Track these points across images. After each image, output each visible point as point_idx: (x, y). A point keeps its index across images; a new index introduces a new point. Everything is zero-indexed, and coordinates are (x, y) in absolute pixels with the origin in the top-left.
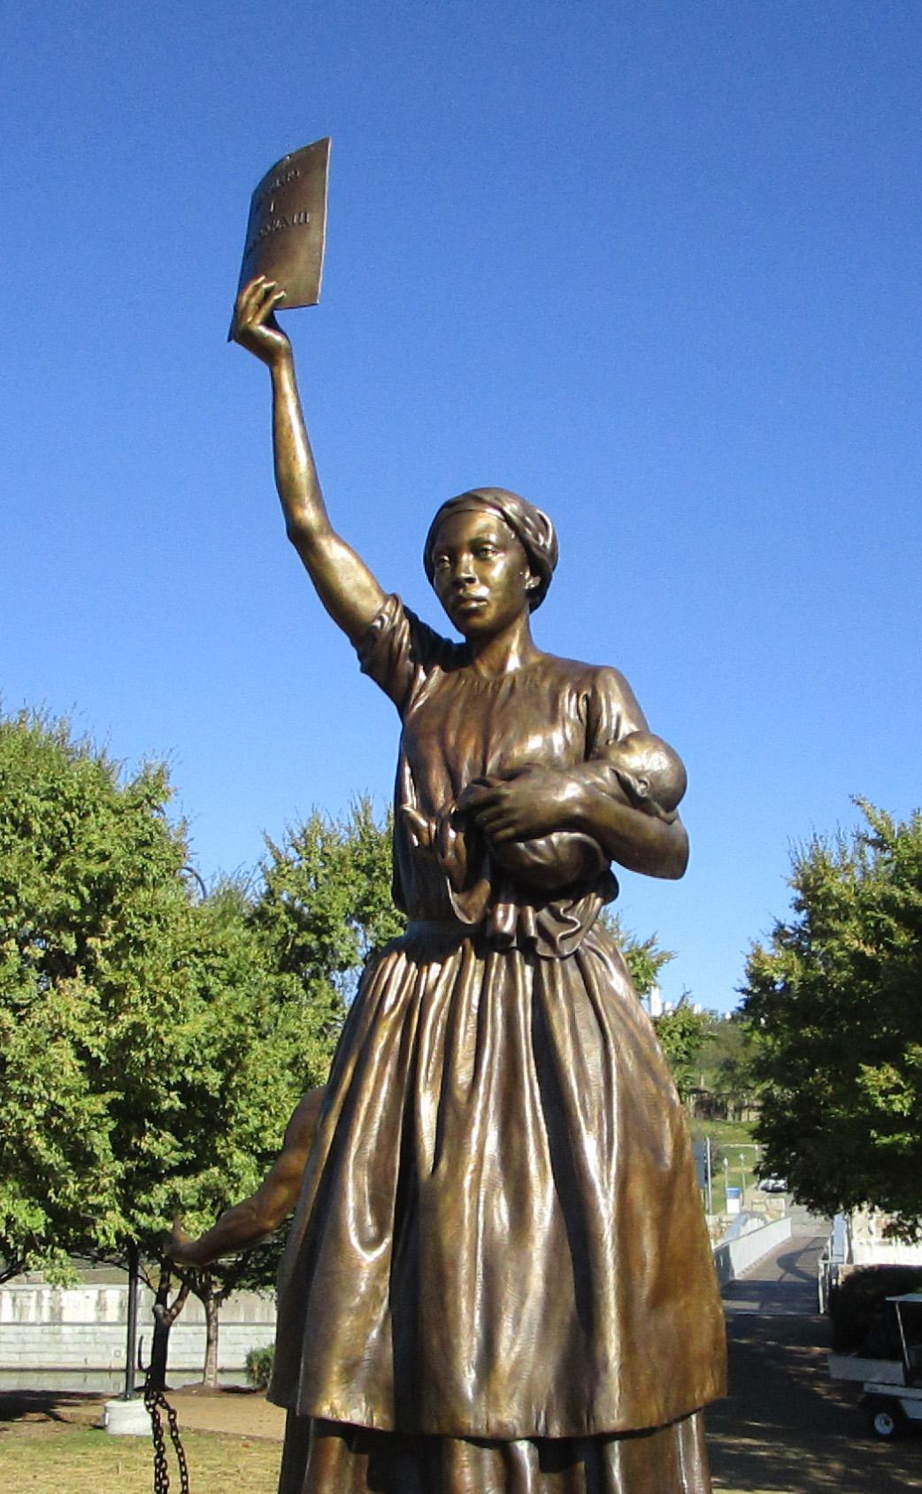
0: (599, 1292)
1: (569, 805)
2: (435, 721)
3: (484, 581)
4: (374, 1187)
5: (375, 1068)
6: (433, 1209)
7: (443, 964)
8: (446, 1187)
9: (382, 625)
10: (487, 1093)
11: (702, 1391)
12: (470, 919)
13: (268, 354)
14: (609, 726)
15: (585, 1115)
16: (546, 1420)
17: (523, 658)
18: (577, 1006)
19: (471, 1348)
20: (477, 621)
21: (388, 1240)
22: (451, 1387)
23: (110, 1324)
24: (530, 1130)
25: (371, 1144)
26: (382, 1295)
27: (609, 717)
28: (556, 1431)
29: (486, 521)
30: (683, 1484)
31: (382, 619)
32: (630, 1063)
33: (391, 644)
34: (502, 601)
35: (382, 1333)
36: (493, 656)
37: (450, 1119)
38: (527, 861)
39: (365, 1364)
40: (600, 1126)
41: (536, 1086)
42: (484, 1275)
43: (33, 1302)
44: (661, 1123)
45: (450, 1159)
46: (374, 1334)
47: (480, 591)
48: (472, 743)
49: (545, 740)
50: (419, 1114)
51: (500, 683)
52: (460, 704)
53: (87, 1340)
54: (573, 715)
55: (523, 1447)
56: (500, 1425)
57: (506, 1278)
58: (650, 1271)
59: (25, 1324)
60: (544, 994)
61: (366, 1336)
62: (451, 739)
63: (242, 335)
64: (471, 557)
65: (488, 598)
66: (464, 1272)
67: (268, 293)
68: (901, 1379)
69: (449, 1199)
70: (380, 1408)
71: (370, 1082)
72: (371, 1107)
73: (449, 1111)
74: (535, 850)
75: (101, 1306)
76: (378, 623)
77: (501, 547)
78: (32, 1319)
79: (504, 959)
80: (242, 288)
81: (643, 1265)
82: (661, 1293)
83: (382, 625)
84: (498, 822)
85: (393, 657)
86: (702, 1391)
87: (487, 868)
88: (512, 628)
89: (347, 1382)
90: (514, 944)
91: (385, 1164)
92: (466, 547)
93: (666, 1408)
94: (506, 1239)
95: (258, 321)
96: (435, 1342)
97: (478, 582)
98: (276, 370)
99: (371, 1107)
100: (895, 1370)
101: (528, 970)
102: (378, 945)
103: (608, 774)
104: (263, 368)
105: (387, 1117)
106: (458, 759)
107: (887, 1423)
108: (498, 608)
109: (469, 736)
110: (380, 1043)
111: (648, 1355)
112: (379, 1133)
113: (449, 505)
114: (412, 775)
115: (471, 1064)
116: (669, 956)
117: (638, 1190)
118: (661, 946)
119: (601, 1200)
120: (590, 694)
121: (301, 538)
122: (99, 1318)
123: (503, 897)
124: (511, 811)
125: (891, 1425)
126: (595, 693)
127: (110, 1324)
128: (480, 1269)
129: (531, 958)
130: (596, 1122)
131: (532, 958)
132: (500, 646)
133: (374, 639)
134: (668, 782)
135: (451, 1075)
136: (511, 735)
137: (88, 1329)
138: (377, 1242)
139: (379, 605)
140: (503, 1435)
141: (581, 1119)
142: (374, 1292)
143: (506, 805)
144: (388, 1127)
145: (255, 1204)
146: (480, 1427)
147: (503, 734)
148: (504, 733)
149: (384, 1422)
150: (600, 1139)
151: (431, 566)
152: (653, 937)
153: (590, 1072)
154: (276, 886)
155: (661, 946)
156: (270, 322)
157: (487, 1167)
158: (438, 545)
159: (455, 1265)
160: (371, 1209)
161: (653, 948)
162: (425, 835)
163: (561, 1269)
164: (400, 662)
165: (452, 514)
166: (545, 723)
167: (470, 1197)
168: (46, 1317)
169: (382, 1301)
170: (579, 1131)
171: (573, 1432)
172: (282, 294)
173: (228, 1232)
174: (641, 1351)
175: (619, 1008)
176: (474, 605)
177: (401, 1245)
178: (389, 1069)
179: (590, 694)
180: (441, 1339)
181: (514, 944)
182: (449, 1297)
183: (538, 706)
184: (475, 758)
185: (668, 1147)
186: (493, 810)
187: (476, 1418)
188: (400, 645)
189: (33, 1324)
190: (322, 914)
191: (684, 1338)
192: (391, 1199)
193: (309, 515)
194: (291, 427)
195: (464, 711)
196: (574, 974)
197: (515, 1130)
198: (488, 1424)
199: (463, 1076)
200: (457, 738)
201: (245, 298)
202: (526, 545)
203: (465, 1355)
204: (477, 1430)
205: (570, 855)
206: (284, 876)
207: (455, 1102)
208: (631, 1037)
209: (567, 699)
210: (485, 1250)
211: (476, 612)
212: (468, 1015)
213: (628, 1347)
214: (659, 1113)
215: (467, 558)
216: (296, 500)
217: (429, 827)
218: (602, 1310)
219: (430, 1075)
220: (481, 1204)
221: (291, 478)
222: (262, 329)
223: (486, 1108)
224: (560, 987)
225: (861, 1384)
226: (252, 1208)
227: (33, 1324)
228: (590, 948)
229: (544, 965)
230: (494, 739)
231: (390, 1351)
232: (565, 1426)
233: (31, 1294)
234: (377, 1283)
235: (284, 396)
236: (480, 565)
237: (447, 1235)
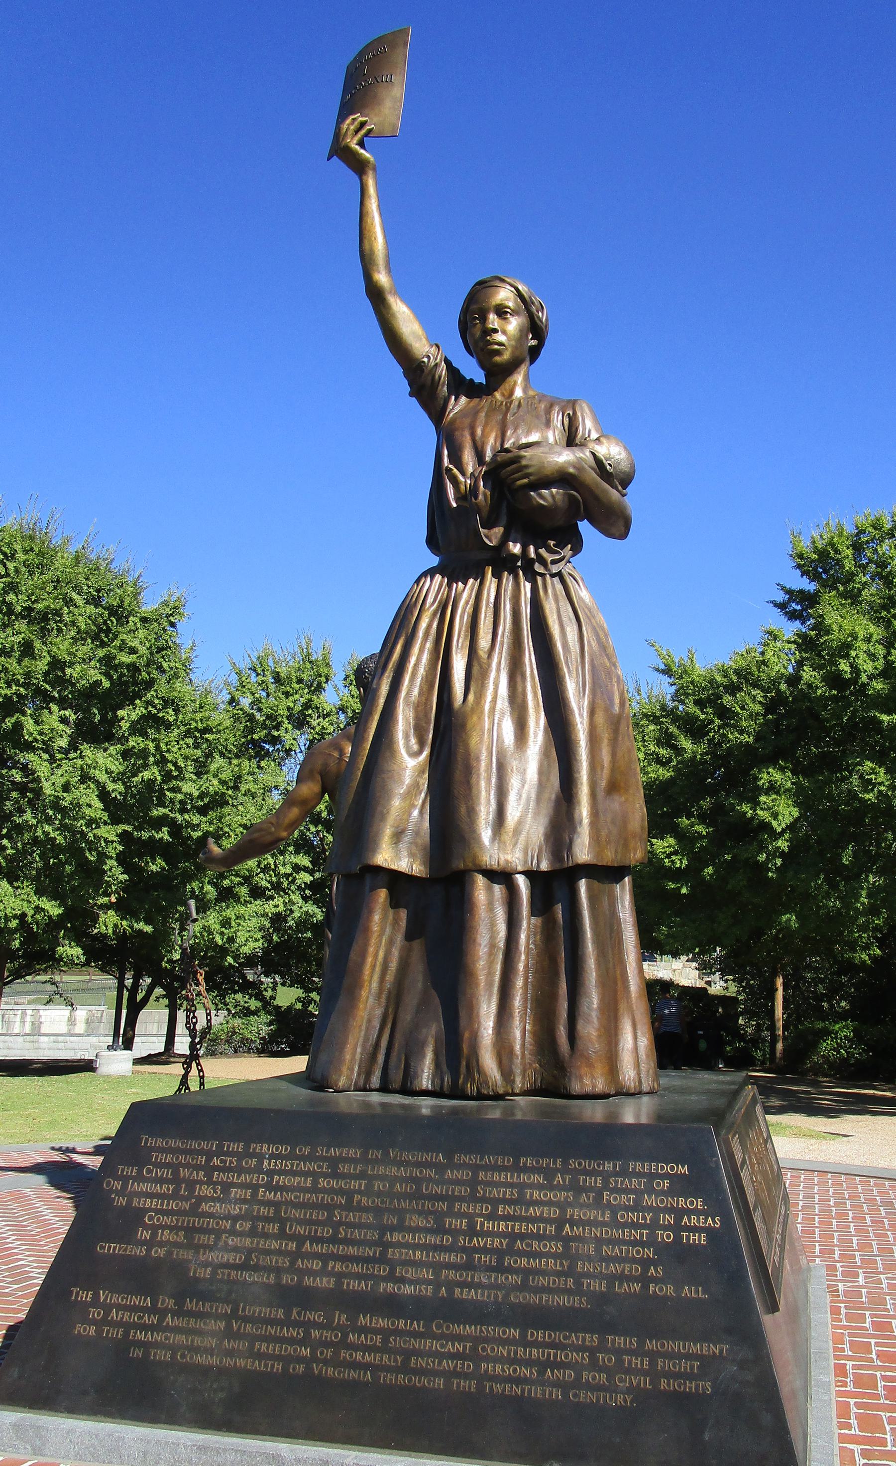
0: (576, 775)
1: (566, 465)
2: (467, 421)
3: (504, 332)
4: (417, 719)
5: (419, 641)
6: (463, 726)
7: (465, 584)
8: (473, 710)
9: (429, 361)
10: (501, 653)
11: (634, 855)
12: (491, 542)
13: (359, 167)
14: (584, 434)
15: (568, 668)
16: (538, 860)
17: (525, 390)
18: (561, 604)
19: (488, 813)
20: (497, 359)
21: (426, 753)
22: (474, 839)
23: (79, 1035)
24: (529, 679)
25: (416, 692)
26: (421, 788)
27: (584, 429)
28: (544, 866)
29: (504, 295)
31: (429, 357)
32: (594, 644)
33: (434, 376)
34: (515, 348)
35: (421, 813)
36: (506, 386)
37: (475, 670)
38: (534, 503)
39: (409, 833)
40: (577, 674)
41: (532, 653)
42: (497, 769)
43: (18, 1018)
44: (613, 686)
45: (475, 693)
46: (416, 813)
47: (500, 337)
48: (493, 435)
49: (542, 437)
50: (452, 667)
51: (511, 403)
52: (483, 414)
53: (60, 1047)
54: (559, 425)
55: (521, 881)
56: (507, 861)
57: (512, 771)
58: (606, 772)
59: (11, 1035)
60: (539, 595)
61: (410, 815)
62: (479, 431)
63: (340, 151)
64: (496, 317)
65: (506, 344)
66: (483, 764)
67: (363, 125)
69: (475, 718)
70: (418, 862)
71: (416, 650)
72: (417, 665)
73: (475, 664)
74: (542, 497)
75: (72, 1021)
76: (426, 360)
77: (515, 313)
78: (16, 1031)
79: (511, 577)
80: (342, 117)
81: (602, 767)
82: (613, 787)
83: (429, 361)
85: (435, 384)
86: (634, 855)
87: (504, 510)
88: (519, 370)
89: (395, 843)
90: (519, 564)
91: (426, 704)
92: (492, 309)
93: (616, 857)
94: (512, 746)
95: (355, 142)
96: (463, 810)
97: (500, 333)
98: (364, 177)
99: (417, 665)
101: (528, 586)
103: (588, 454)
104: (355, 178)
105: (427, 675)
106: (483, 444)
108: (513, 352)
109: (491, 431)
110: (423, 624)
111: (606, 822)
112: (421, 684)
113: (480, 283)
114: (449, 456)
115: (490, 636)
117: (600, 718)
119: (578, 719)
120: (571, 414)
121: (376, 296)
122: (70, 1030)
123: (513, 535)
124: (526, 467)
126: (575, 413)
127: (79, 1035)
128: (494, 765)
129: (529, 576)
130: (575, 672)
131: (531, 576)
132: (510, 380)
133: (422, 371)
134: (624, 466)
135: (476, 645)
136: (520, 431)
137: (61, 1038)
138: (420, 752)
139: (427, 349)
140: (508, 870)
141: (565, 670)
142: (416, 785)
143: (524, 462)
144: (428, 682)
145: (274, 821)
146: (493, 863)
147: (515, 431)
148: (515, 430)
149: (420, 871)
150: (577, 683)
151: (464, 328)
153: (571, 644)
154: (238, 695)
156: (361, 144)
157: (499, 702)
158: (474, 307)
159: (478, 760)
160: (414, 733)
162: (463, 487)
163: (549, 765)
164: (440, 387)
165: (482, 288)
166: (543, 427)
167: (489, 718)
168: (28, 1030)
169: (421, 794)
170: (563, 677)
172: (373, 126)
173: (251, 841)
174: (602, 817)
175: (586, 610)
176: (496, 347)
177: (434, 758)
178: (429, 645)
179: (571, 414)
180: (468, 808)
181: (519, 564)
182: (474, 781)
183: (538, 417)
184: (495, 443)
185: (617, 700)
186: (514, 466)
187: (491, 856)
188: (440, 377)
189: (17, 1035)
190: (272, 714)
191: (625, 822)
192: (430, 725)
193: (382, 278)
194: (373, 217)
195: (487, 416)
196: (559, 587)
197: (519, 679)
198: (498, 862)
199: (484, 642)
200: (483, 432)
201: (345, 126)
202: (531, 317)
203: (483, 817)
204: (491, 865)
205: (563, 501)
206: (244, 687)
207: (479, 658)
208: (594, 628)
209: (556, 415)
210: (498, 753)
211: (498, 353)
212: (487, 607)
213: (595, 813)
214: (611, 679)
215: (492, 317)
216: (375, 268)
217: (465, 482)
218: (579, 786)
219: (460, 645)
220: (496, 725)
221: (372, 251)
222: (358, 147)
223: (499, 663)
224: (550, 591)
226: (272, 824)
227: (17, 1035)
228: (570, 574)
229: (539, 579)
230: (509, 433)
231: (426, 824)
232: (552, 863)
233: (16, 1012)
234: (419, 779)
235: (369, 197)
236: (502, 322)
237: (473, 741)
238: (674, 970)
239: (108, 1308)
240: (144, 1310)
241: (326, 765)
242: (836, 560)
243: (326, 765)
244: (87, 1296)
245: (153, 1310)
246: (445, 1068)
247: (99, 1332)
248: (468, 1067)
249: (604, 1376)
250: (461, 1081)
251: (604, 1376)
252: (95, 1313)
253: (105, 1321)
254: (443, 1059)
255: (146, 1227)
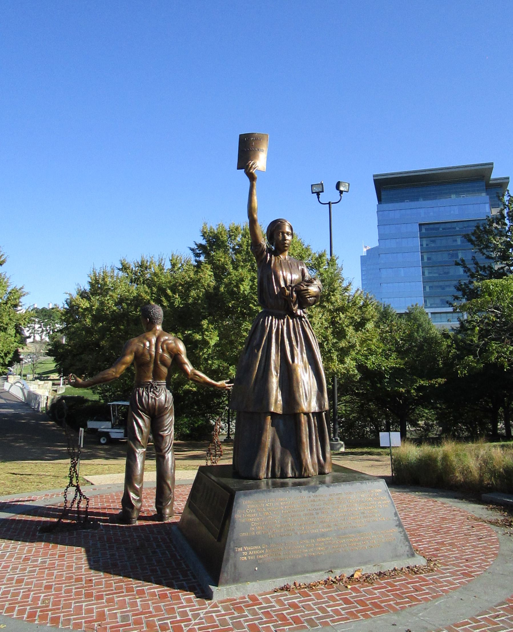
30: (203, 440)
68: (110, 427)
84: (307, 294)
96: (298, 395)
100: (109, 424)
102: (247, 296)
107: (104, 440)
116: (28, 293)
118: (25, 290)
124: (309, 292)
125: (106, 440)
152: (23, 287)
155: (25, 290)
161: (22, 290)
171: (320, 411)
186: (306, 291)
225: (97, 429)
238: (39, 385)
239: (248, 551)
240: (259, 550)
241: (138, 349)
242: (251, 258)
243: (138, 349)
244: (241, 549)
245: (262, 549)
246: (295, 470)
247: (248, 558)
248: (305, 469)
249: (245, 558)
250: (303, 473)
251: (245, 558)
252: (245, 553)
253: (248, 555)
254: (294, 467)
255: (253, 527)
